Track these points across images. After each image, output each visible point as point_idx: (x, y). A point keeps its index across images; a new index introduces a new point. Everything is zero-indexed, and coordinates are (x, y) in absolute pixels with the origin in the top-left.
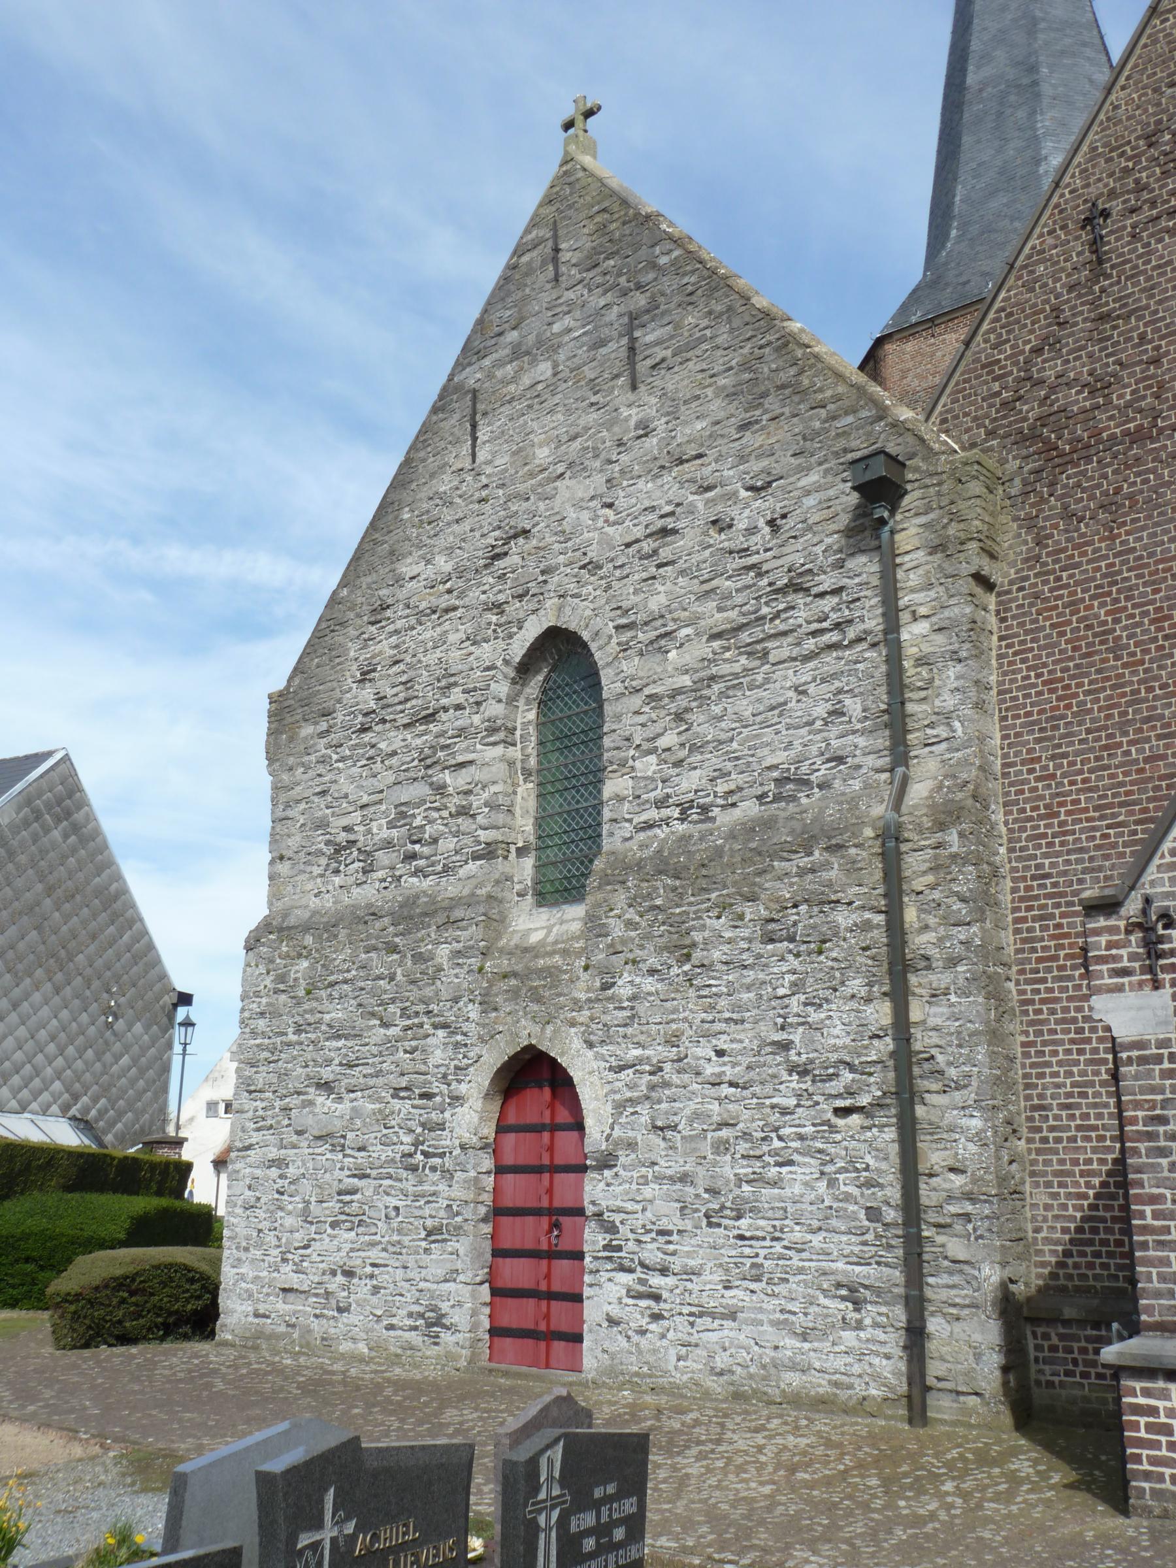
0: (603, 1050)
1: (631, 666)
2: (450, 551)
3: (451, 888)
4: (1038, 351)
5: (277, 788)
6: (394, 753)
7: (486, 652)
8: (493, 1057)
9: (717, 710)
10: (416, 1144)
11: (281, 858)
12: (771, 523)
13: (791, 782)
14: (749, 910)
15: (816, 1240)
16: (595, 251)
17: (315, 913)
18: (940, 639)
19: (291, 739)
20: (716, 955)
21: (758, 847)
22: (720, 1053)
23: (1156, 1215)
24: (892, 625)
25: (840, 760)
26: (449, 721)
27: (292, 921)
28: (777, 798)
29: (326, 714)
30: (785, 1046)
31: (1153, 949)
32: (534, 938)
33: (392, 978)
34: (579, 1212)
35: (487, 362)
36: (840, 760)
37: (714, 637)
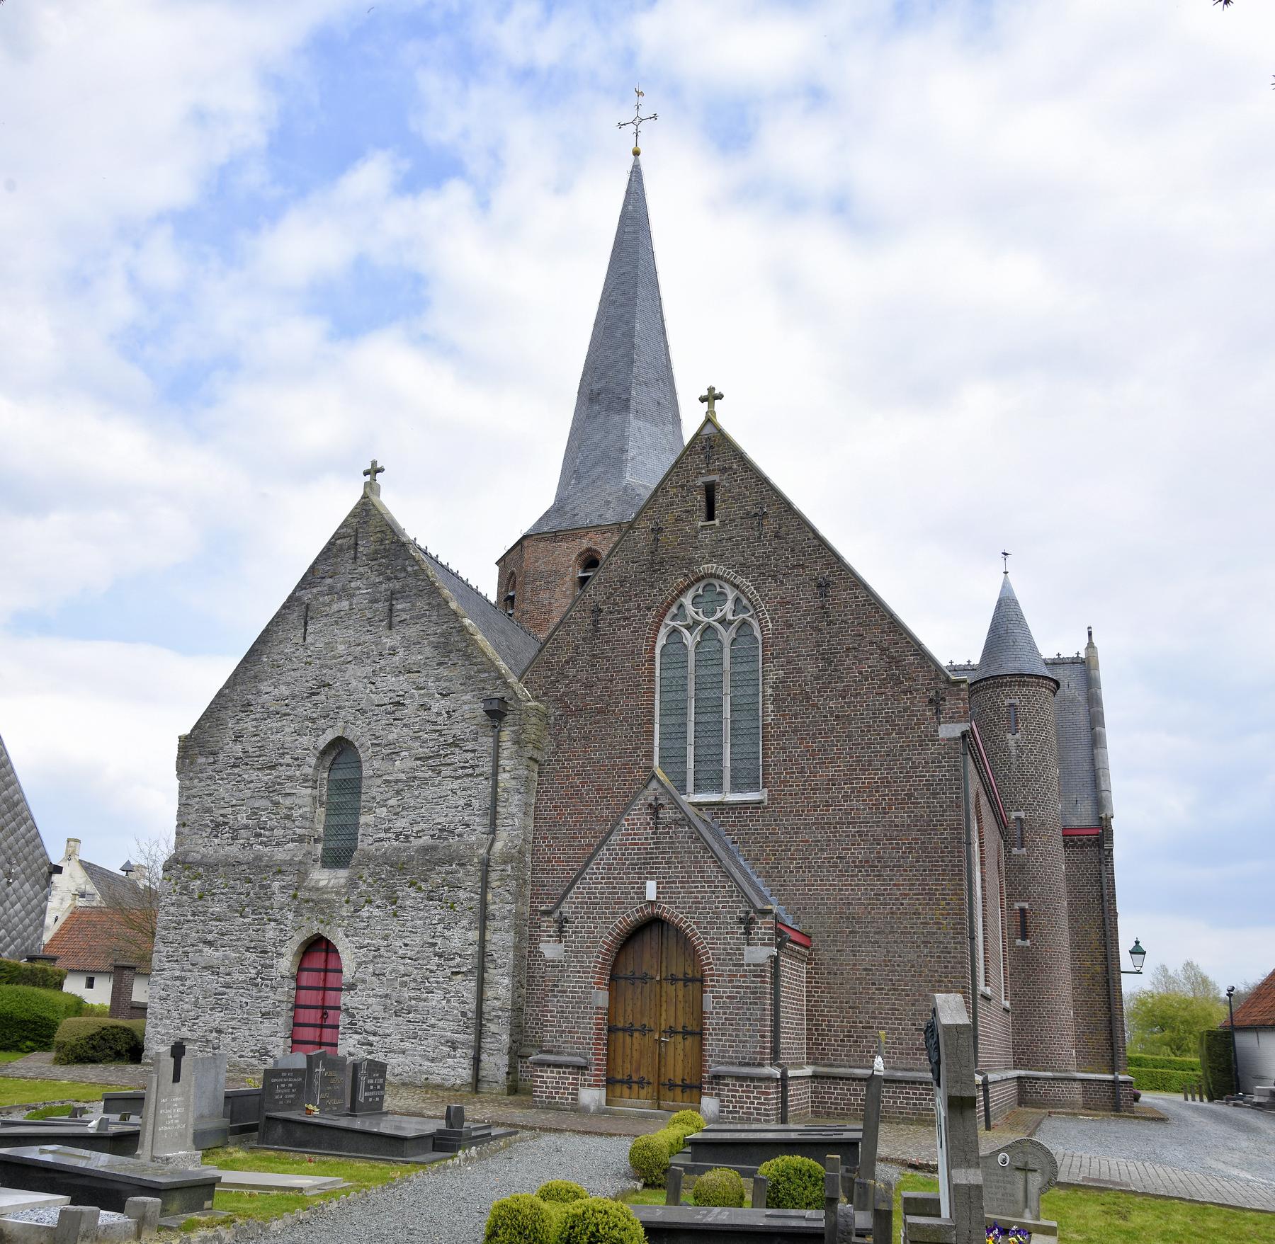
0: (354, 939)
1: (377, 764)
2: (288, 684)
3: (280, 855)
4: (567, 662)
5: (182, 788)
7: (305, 740)
8: (299, 938)
9: (416, 793)
10: (258, 974)
11: (184, 825)
12: (448, 712)
13: (446, 831)
14: (423, 886)
15: (440, 1024)
16: (376, 552)
17: (204, 856)
18: (513, 782)
19: (192, 763)
20: (407, 903)
21: (432, 858)
22: (406, 945)
24: (495, 774)
25: (468, 826)
26: (283, 772)
27: (190, 859)
28: (439, 837)
29: (214, 753)
30: (434, 945)
31: (561, 930)
32: (322, 883)
33: (248, 894)
34: (338, 1008)
35: (315, 590)
36: (468, 826)
37: (419, 759)
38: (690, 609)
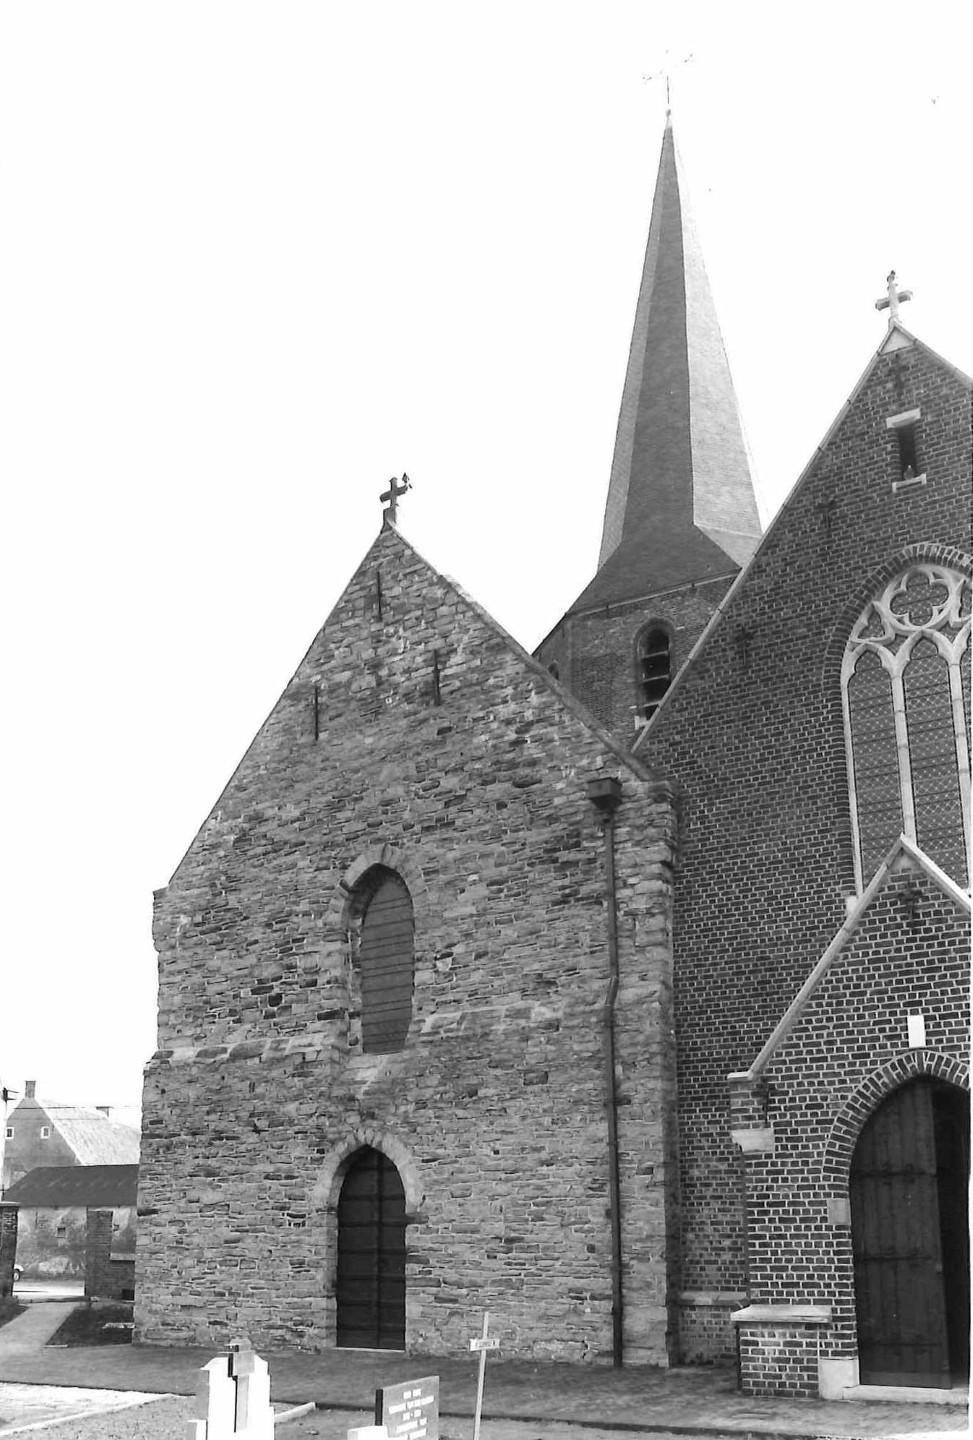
6: (256, 942)
22: (496, 1152)
23: (761, 1245)
37: (492, 884)
38: (888, 617)
